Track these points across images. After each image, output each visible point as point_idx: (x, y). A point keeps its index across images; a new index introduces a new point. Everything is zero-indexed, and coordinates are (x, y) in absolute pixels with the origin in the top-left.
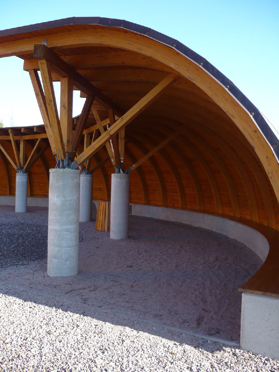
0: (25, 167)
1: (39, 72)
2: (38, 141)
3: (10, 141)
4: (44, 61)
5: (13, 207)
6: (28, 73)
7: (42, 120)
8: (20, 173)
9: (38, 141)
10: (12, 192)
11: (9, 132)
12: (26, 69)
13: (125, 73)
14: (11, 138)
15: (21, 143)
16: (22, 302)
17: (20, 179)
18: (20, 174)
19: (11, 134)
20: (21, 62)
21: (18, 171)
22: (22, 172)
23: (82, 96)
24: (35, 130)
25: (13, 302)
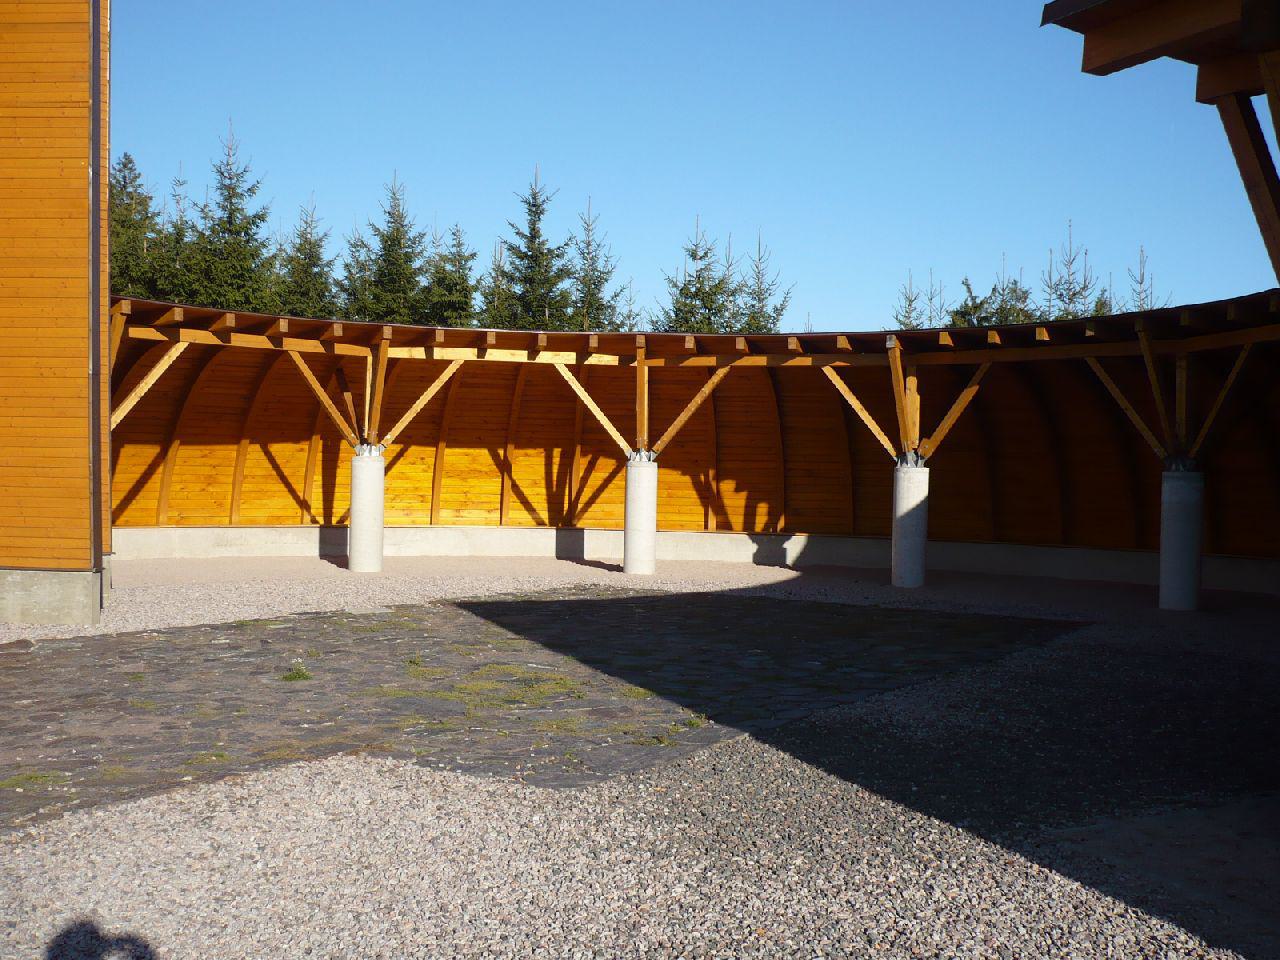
0: (1196, 448)
1: (1261, 104)
2: (1243, 355)
3: (1140, 359)
4: (488, 342)
5: (1152, 592)
6: (1212, 111)
7: (1273, 274)
8: (1177, 470)
9: (1243, 355)
10: (1146, 538)
11: (1137, 329)
12: (1203, 96)
13: (386, 606)
14: (1143, 347)
15: (1178, 364)
16: (1200, 945)
17: (1176, 493)
18: (1177, 474)
19: (1141, 335)
20: (1187, 73)
21: (1171, 465)
22: (1184, 466)
23: (737, 490)
24: (1231, 315)
25: (1166, 941)
